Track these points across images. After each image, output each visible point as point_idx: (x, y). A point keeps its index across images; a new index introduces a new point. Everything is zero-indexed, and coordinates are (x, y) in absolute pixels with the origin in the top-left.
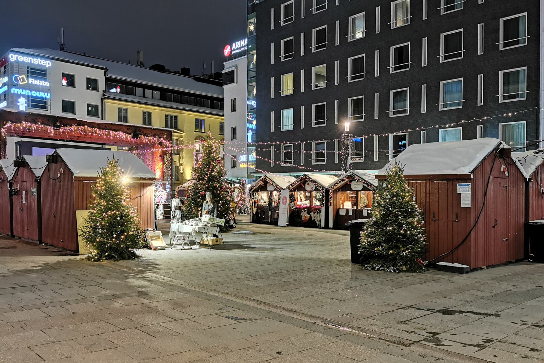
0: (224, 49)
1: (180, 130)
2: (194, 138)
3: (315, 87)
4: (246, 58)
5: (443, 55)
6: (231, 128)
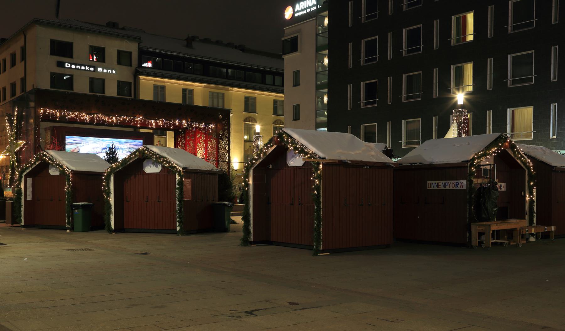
0: (284, 11)
2: (243, 119)
4: (315, 21)
5: (364, 58)
6: (293, 106)
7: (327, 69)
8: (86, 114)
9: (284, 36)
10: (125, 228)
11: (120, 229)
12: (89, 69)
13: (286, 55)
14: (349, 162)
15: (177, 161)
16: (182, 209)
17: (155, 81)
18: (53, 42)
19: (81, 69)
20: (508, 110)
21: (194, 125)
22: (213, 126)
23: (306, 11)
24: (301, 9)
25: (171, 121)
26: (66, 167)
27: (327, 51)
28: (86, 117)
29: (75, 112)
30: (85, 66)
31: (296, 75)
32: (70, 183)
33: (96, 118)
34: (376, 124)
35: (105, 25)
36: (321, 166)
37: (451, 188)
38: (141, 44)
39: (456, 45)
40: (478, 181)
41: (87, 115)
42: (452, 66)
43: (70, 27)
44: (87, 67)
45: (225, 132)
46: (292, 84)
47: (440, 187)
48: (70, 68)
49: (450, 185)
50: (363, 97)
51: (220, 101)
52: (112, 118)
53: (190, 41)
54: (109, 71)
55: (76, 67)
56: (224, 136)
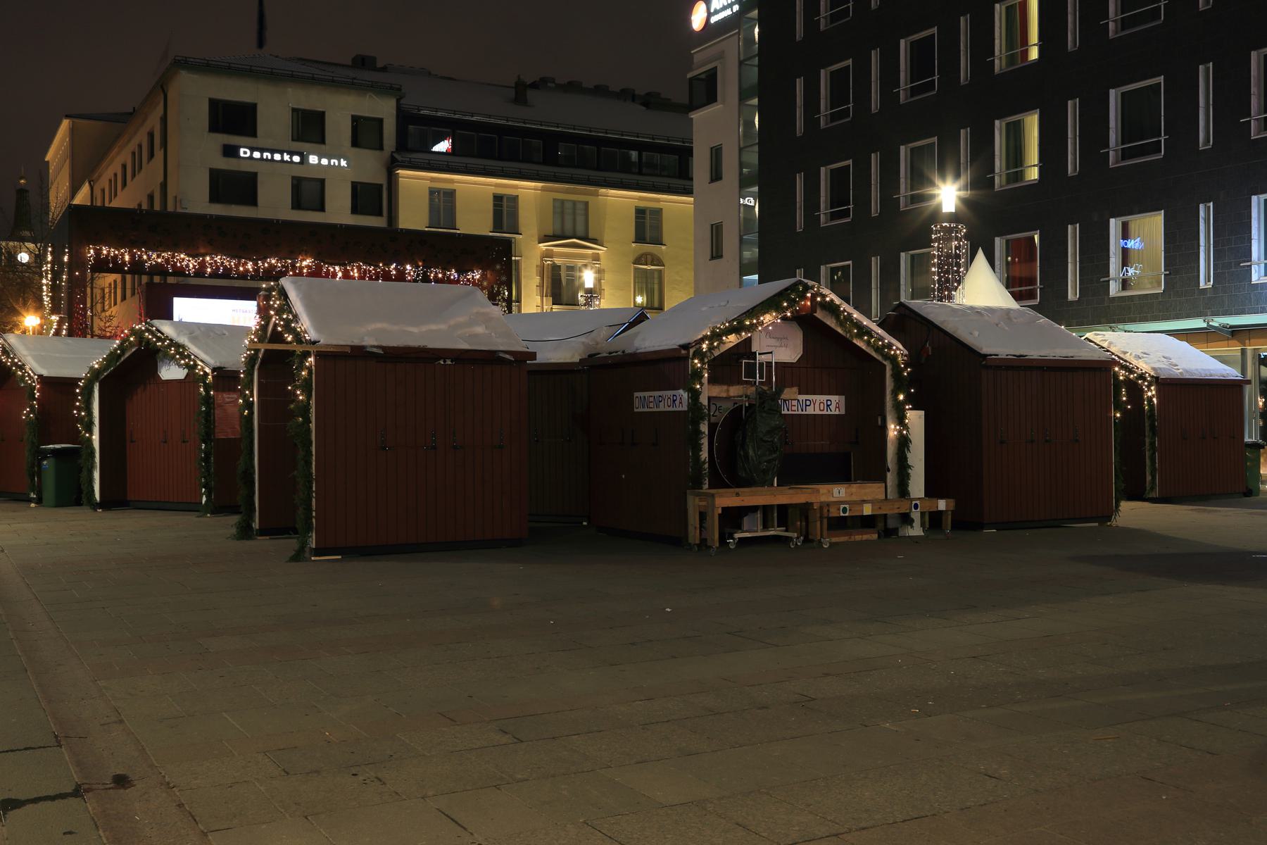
1: (594, 241)
2: (632, 259)
3: (829, 120)
6: (709, 228)
7: (757, 141)
8: (188, 255)
9: (691, 70)
10: (128, 499)
11: (115, 500)
12: (291, 158)
13: (701, 109)
14: (375, 350)
15: (206, 353)
16: (212, 458)
17: (432, 180)
18: (214, 104)
19: (272, 160)
20: (1112, 221)
21: (432, 275)
22: (478, 277)
23: (732, 10)
24: (721, 6)
25: (380, 268)
26: (31, 369)
27: (757, 99)
28: (189, 263)
29: (164, 252)
30: (281, 153)
31: (716, 153)
32: (35, 402)
33: (211, 264)
34: (850, 262)
35: (350, 63)
36: (311, 359)
37: (818, 412)
38: (402, 101)
39: (1006, 72)
40: (728, 391)
41: (191, 259)
42: (997, 122)
43: (251, 71)
44: (285, 154)
45: (501, 289)
46: (707, 176)
47: (794, 408)
48: (251, 158)
49: (814, 404)
50: (826, 202)
51: (580, 219)
52: (245, 264)
53: (521, 92)
54: (332, 161)
55: (262, 155)
56: (500, 297)
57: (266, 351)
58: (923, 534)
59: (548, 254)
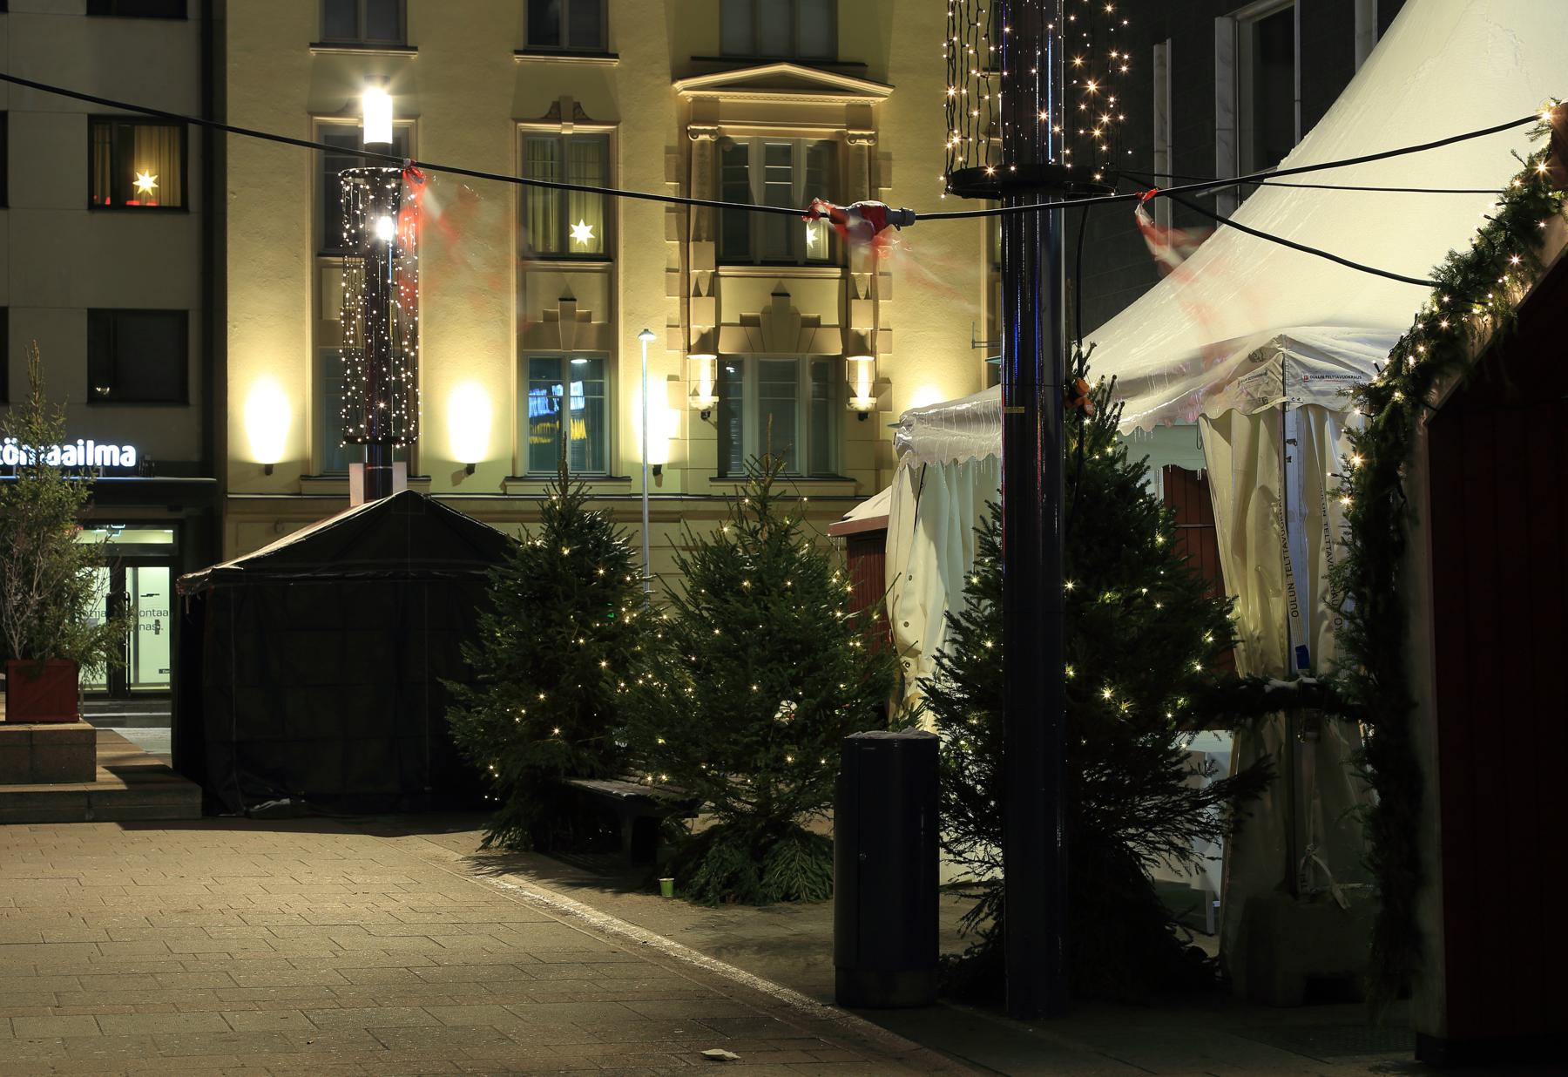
1: (856, 69)
57: (1340, 881)
58: (171, 767)
59: (703, 113)
